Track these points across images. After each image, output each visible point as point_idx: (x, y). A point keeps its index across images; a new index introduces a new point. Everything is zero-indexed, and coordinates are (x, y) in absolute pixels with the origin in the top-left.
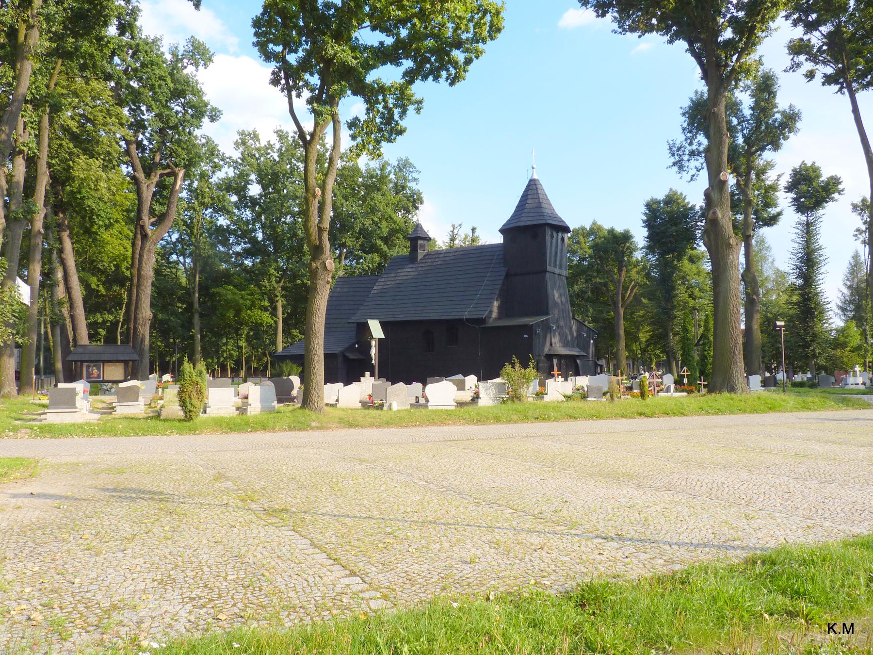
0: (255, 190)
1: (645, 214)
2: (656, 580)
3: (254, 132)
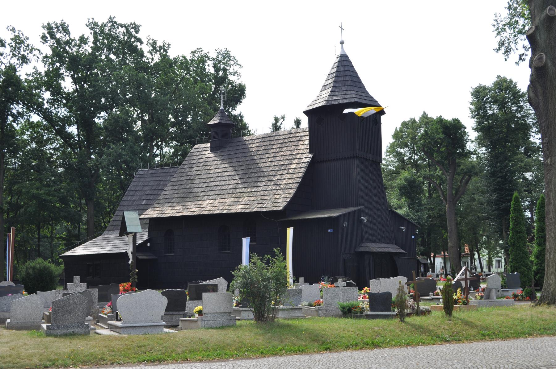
0: (68, 84)
1: (472, 104)
2: (517, 299)
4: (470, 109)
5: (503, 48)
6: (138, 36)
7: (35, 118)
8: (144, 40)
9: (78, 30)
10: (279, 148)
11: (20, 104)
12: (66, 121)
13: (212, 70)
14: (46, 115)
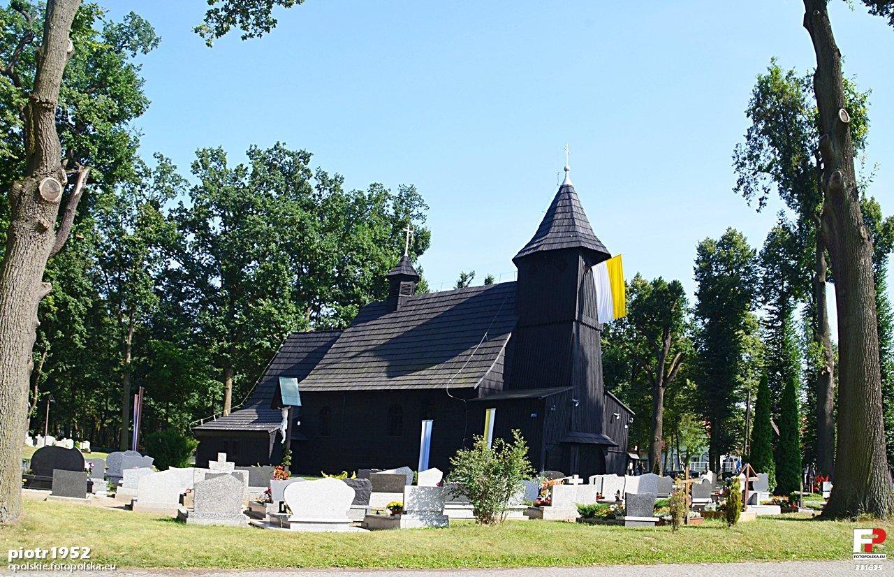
3: (219, 151)
4: (695, 269)
5: (742, 187)
6: (307, 167)
7: (175, 265)
8: (314, 173)
9: (236, 158)
10: (414, 310)
11: (159, 246)
12: (210, 270)
13: (392, 212)
14: (187, 260)
